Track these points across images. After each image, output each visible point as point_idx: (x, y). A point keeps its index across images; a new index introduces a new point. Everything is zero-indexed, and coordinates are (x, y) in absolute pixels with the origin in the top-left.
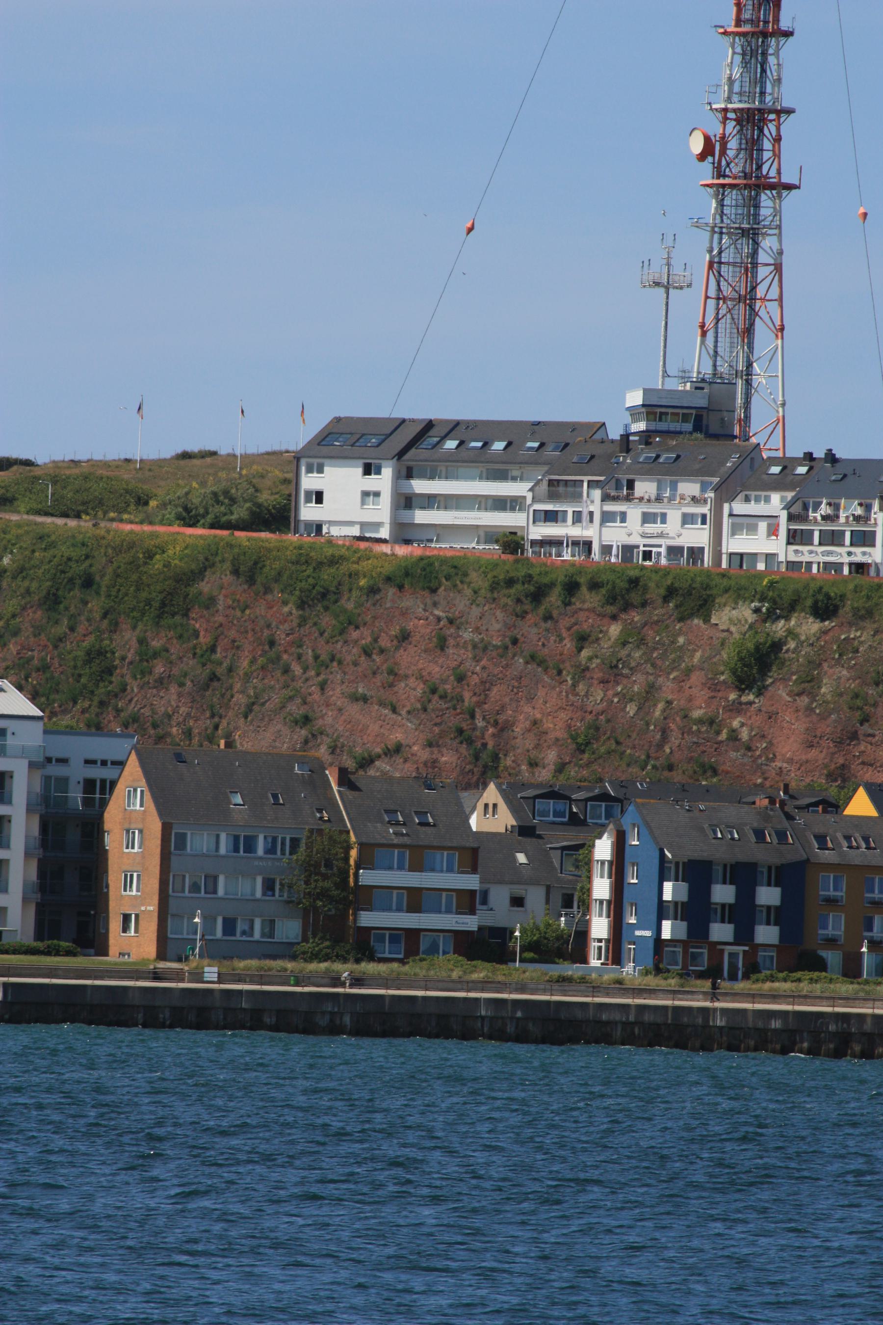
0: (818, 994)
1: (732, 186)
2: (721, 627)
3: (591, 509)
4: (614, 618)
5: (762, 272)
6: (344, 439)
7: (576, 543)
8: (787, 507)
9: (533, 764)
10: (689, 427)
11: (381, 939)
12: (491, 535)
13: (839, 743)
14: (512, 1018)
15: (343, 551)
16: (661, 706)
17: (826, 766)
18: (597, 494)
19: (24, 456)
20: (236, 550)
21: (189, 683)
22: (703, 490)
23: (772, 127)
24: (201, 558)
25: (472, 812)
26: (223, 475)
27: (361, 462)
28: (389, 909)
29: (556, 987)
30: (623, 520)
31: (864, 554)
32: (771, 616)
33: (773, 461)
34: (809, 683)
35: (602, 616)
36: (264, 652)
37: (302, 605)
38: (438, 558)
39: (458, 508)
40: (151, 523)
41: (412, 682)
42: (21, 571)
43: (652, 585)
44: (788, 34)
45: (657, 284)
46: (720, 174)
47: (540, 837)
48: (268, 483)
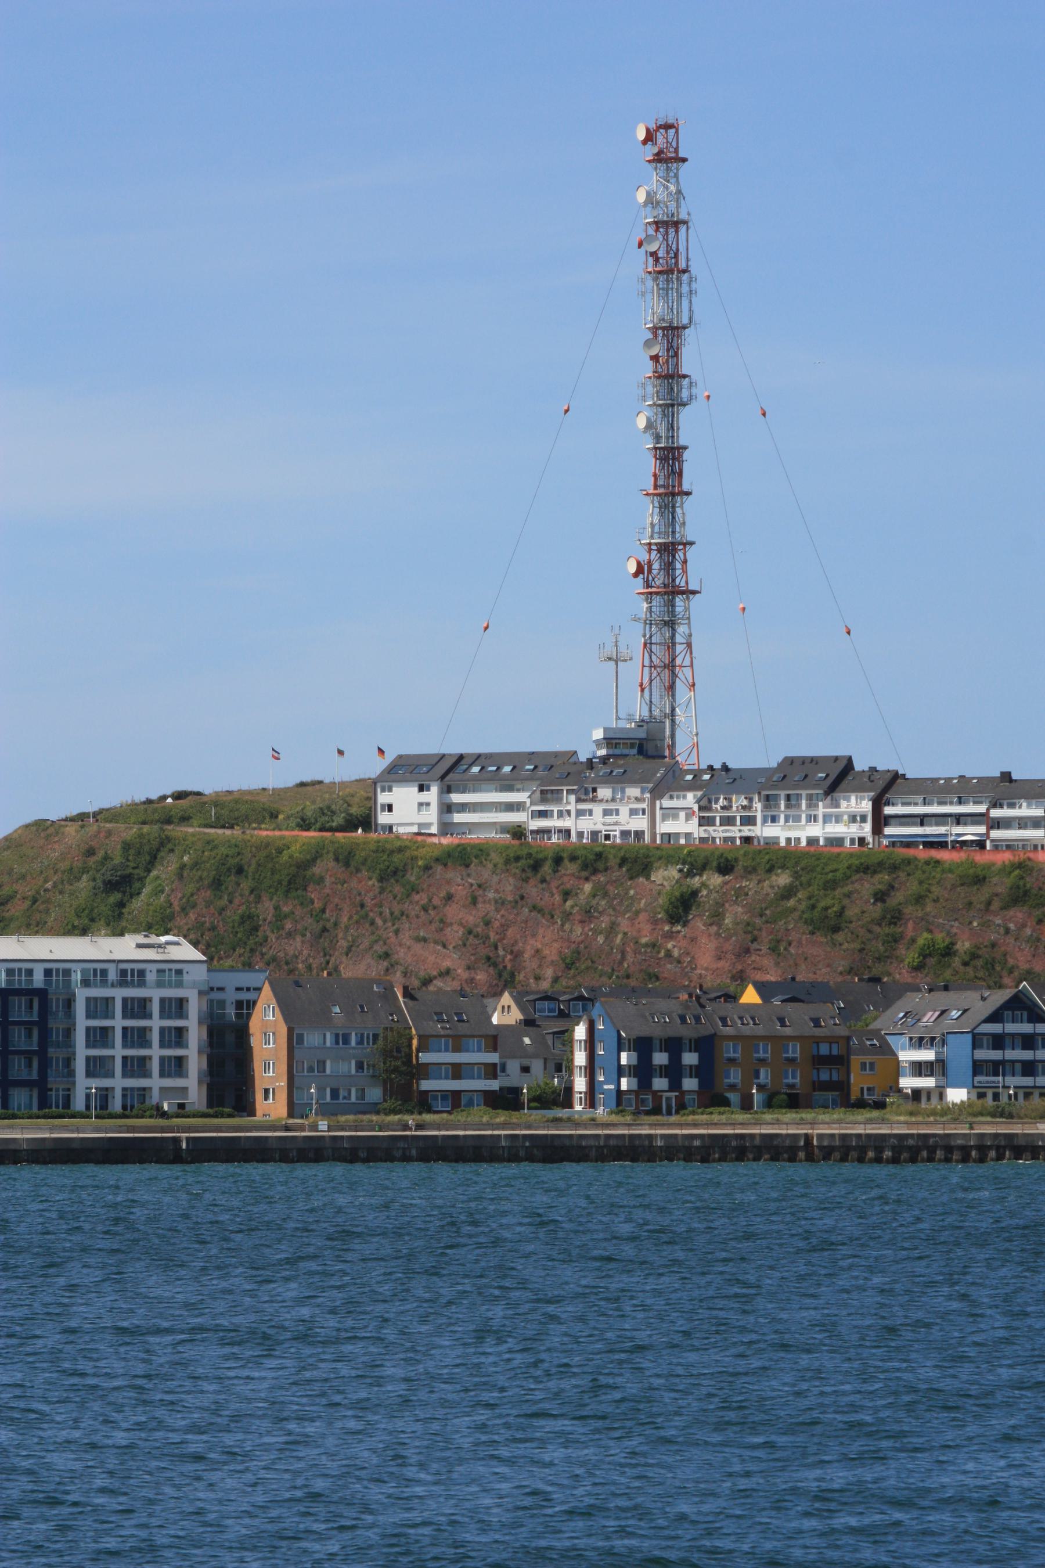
0: (724, 1121)
1: (657, 593)
2: (658, 883)
3: (568, 808)
4: (587, 879)
5: (679, 648)
6: (407, 769)
7: (560, 831)
8: (698, 801)
9: (537, 978)
10: (635, 751)
11: (435, 1098)
12: (505, 828)
13: (738, 956)
14: (523, 1147)
15: (407, 843)
16: (620, 936)
17: (730, 971)
18: (572, 798)
19: (196, 789)
20: (336, 845)
21: (308, 934)
22: (643, 792)
23: (681, 553)
24: (313, 851)
25: (494, 1011)
26: (327, 796)
27: (417, 784)
28: (440, 1078)
29: (551, 1125)
30: (591, 814)
31: (750, 830)
32: (690, 874)
33: (689, 772)
34: (717, 917)
35: (579, 878)
36: (357, 912)
37: (381, 879)
38: (468, 844)
39: (482, 811)
40: (280, 830)
41: (455, 927)
42: (196, 865)
43: (611, 856)
44: (688, 494)
45: (610, 659)
46: (648, 586)
47: (538, 1026)
48: (356, 799)
